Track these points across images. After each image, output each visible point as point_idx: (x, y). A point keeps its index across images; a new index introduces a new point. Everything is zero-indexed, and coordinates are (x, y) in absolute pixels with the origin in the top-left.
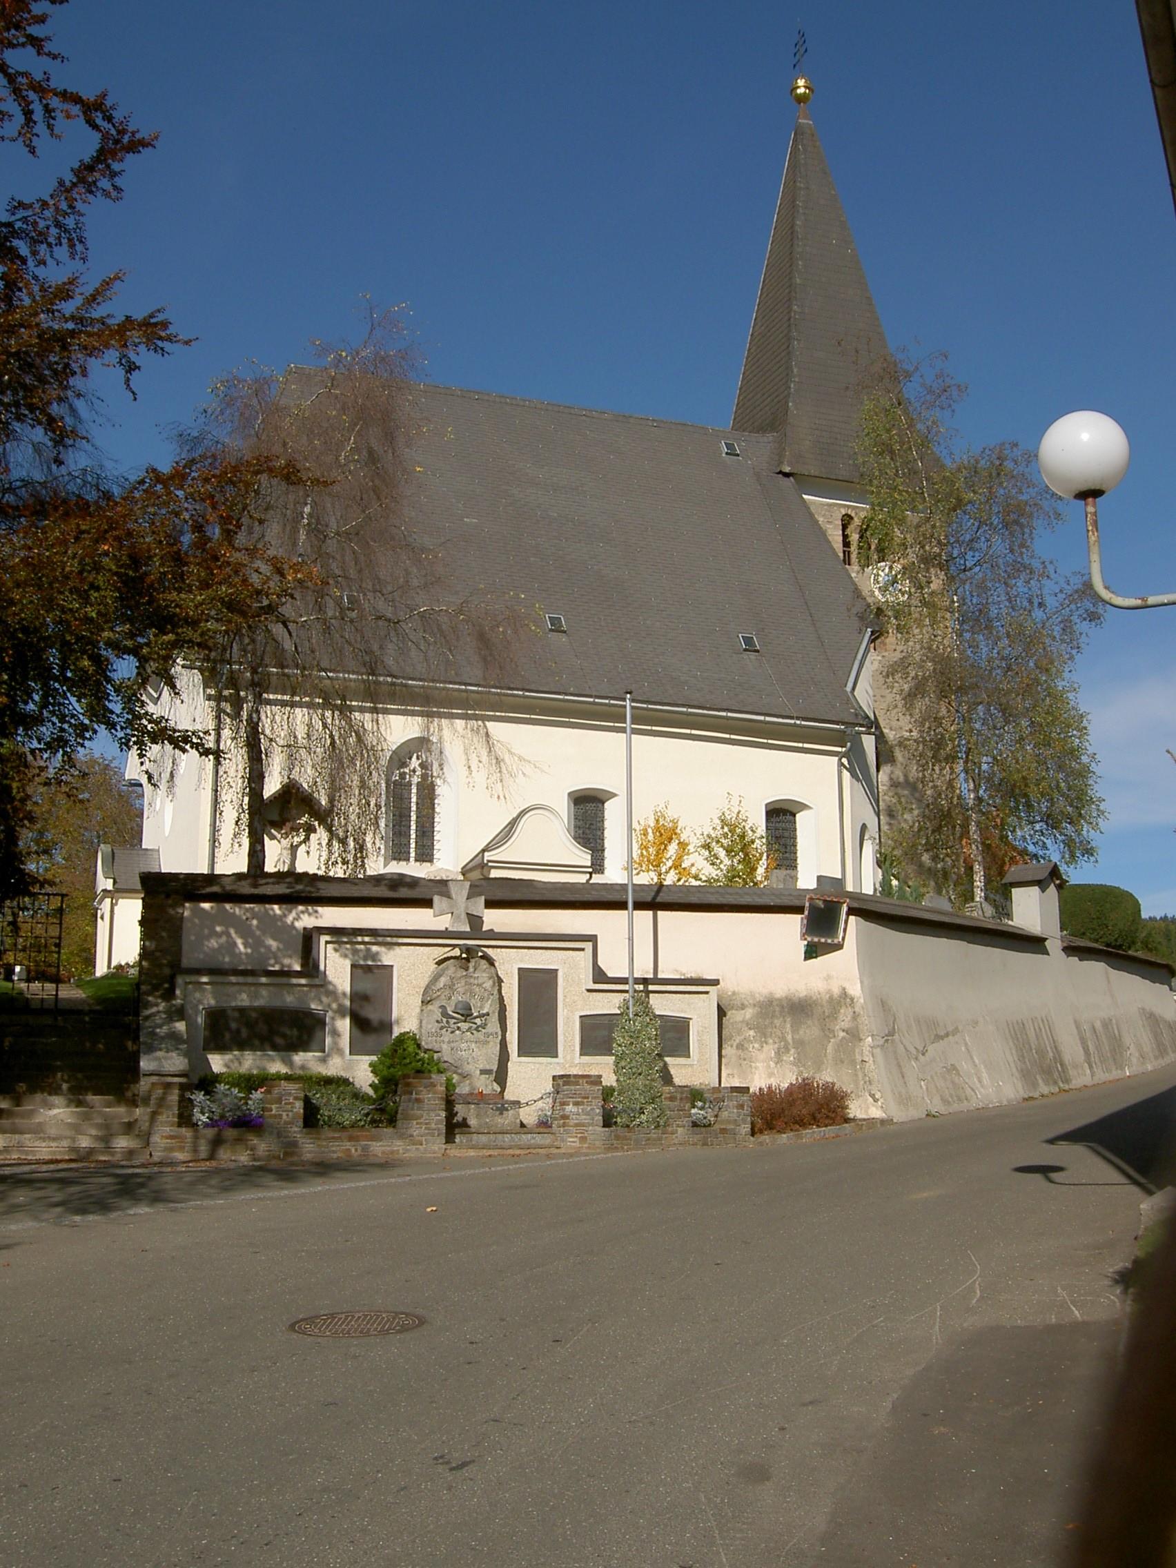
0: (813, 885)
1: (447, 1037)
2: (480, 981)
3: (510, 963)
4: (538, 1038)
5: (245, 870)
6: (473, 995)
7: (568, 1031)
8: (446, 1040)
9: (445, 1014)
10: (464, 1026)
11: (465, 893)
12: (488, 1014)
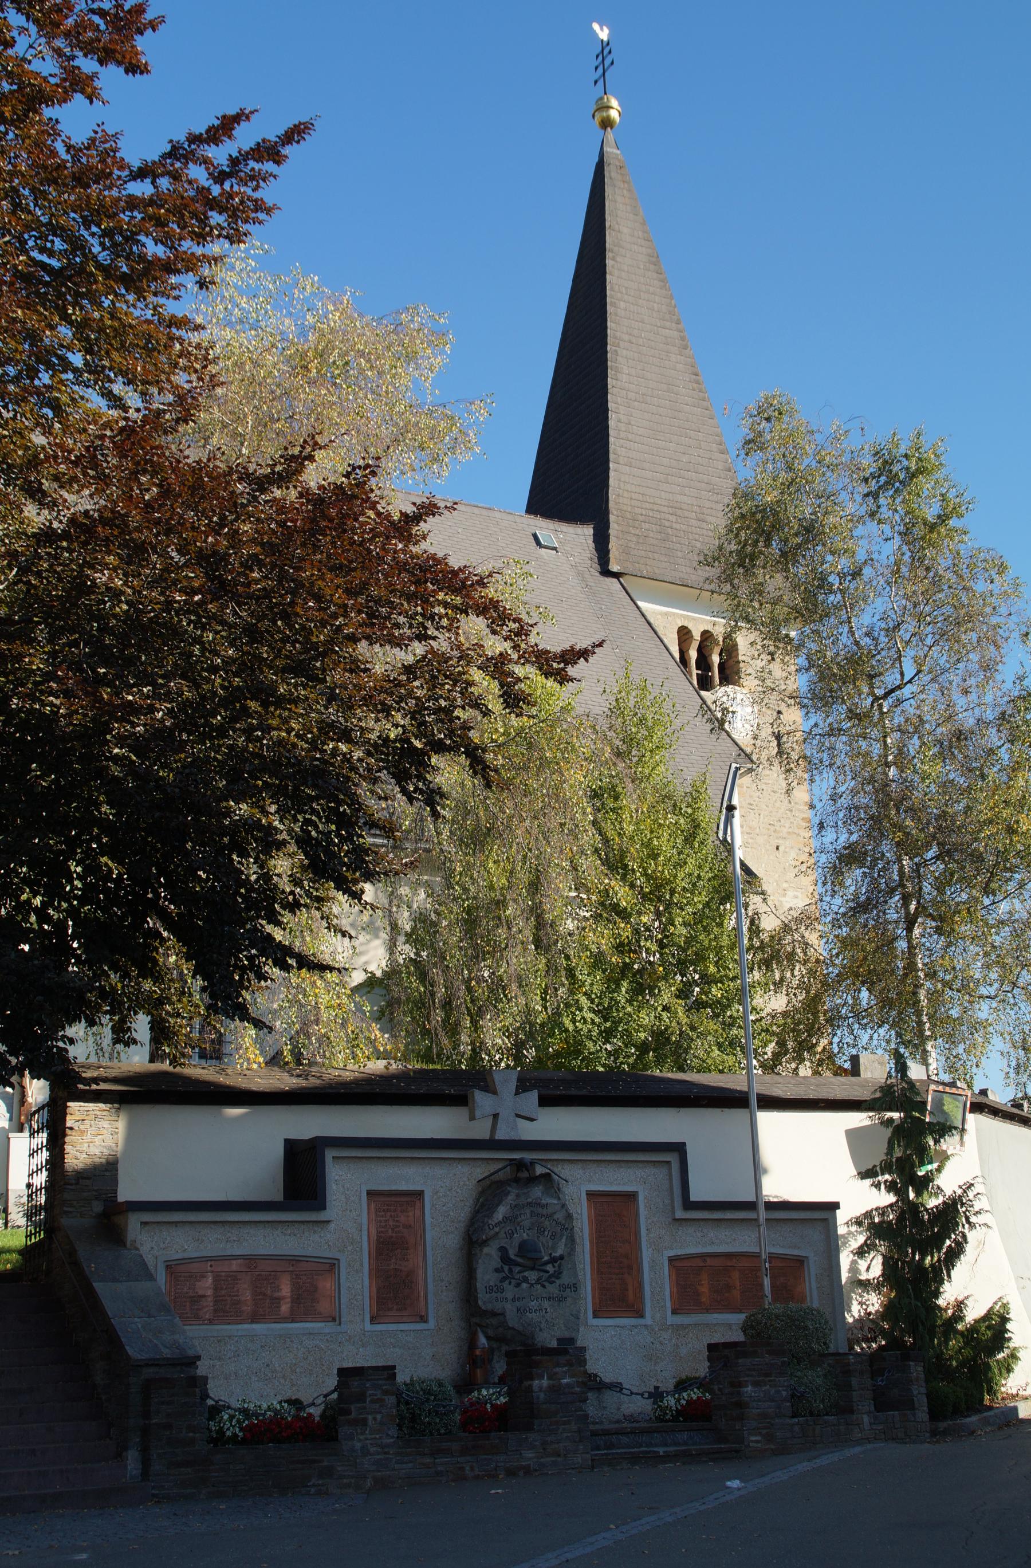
0: (79, 137)
1: (510, 1291)
2: (550, 1210)
3: (579, 1183)
4: (620, 1297)
5: (692, 1199)
6: (541, 1231)
7: (656, 1281)
8: (509, 1295)
9: (505, 1258)
10: (532, 1276)
11: (513, 1085)
12: (561, 1257)
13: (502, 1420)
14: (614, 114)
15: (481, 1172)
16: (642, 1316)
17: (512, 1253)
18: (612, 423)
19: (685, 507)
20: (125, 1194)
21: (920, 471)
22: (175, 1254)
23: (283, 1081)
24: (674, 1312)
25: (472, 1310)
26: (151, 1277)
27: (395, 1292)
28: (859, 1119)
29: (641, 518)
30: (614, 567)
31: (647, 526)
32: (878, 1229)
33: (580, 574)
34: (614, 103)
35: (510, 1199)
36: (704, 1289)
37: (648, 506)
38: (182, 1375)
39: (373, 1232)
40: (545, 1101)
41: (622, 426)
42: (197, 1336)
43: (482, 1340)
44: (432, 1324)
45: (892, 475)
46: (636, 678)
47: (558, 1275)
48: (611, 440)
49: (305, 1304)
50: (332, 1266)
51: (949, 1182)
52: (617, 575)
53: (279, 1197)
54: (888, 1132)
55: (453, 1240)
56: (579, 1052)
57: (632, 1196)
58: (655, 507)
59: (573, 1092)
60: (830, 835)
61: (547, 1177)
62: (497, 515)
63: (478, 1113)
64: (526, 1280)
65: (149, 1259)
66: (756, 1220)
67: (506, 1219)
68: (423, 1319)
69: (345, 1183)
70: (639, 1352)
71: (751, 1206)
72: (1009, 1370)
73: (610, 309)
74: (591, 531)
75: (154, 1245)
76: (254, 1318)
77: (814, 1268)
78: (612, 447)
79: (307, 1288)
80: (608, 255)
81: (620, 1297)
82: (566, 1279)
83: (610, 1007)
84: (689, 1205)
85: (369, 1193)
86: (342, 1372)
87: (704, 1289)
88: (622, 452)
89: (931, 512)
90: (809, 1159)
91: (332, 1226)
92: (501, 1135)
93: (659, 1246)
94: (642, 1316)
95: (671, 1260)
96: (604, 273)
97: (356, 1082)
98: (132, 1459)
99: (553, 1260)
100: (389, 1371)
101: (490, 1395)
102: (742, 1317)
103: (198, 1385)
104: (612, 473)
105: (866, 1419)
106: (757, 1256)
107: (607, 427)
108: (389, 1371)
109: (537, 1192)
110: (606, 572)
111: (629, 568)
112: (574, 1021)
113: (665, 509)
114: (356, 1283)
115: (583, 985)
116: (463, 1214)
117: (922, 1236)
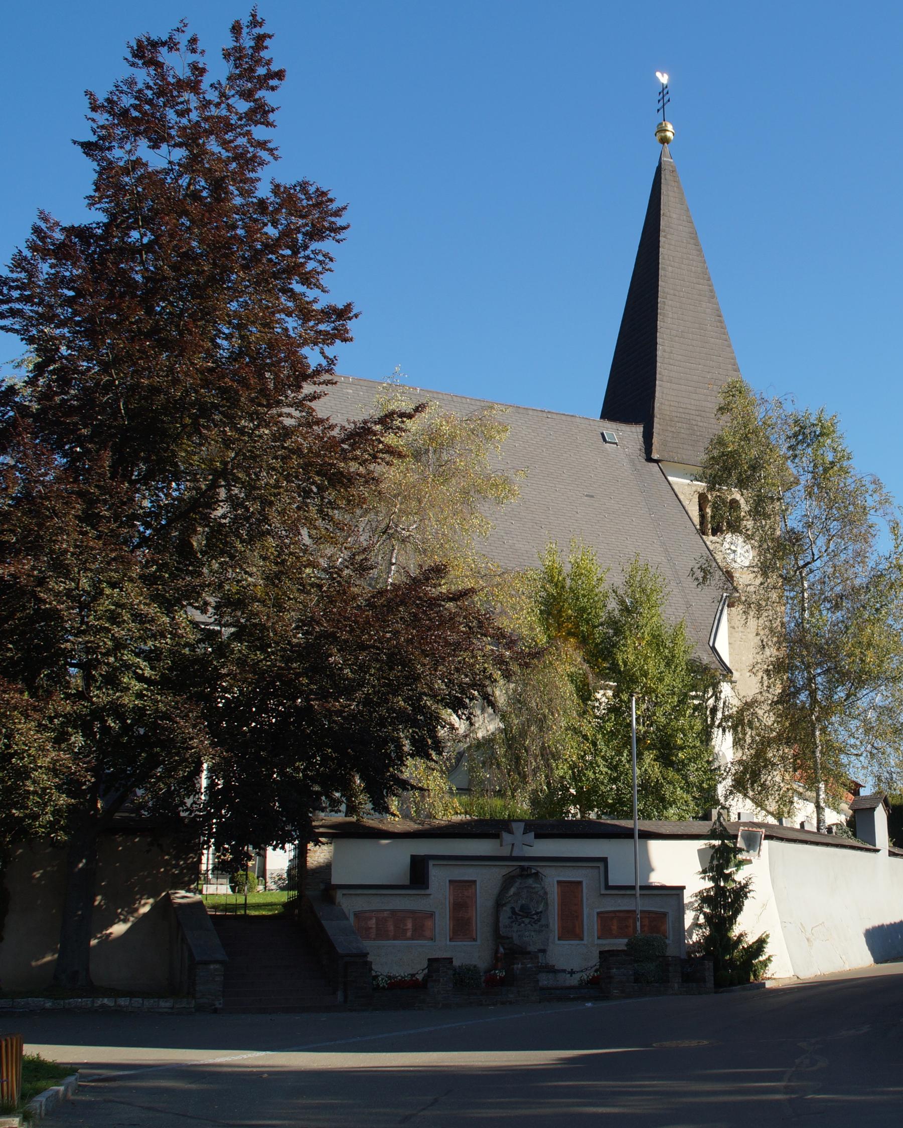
3: (552, 877)
4: (571, 929)
8: (515, 930)
10: (527, 920)
13: (503, 982)
14: (669, 135)
15: (505, 871)
16: (582, 940)
17: (517, 910)
18: (659, 353)
19: (708, 410)
20: (336, 880)
21: (822, 434)
22: (358, 908)
23: (412, 826)
24: (599, 938)
25: (498, 937)
26: (347, 919)
27: (461, 927)
28: (701, 844)
29: (676, 419)
30: (655, 456)
31: (680, 425)
32: (705, 899)
33: (632, 461)
34: (670, 127)
35: (517, 884)
36: (615, 928)
37: (681, 410)
38: (361, 961)
39: (452, 901)
40: (537, 836)
41: (666, 355)
42: (368, 945)
43: (501, 950)
44: (479, 942)
45: (806, 434)
46: (641, 562)
47: (539, 920)
48: (658, 364)
49: (419, 932)
50: (431, 915)
51: (740, 876)
52: (657, 461)
53: (407, 882)
54: (712, 852)
55: (490, 903)
56: (597, 792)
57: (580, 883)
58: (687, 411)
59: (555, 831)
60: (768, 652)
61: (537, 874)
62: (578, 420)
63: (504, 843)
64: (523, 922)
65: (346, 911)
66: (635, 895)
67: (514, 894)
68: (475, 940)
69: (438, 876)
70: (573, 957)
71: (633, 888)
72: (766, 966)
73: (661, 272)
74: (642, 429)
75: (349, 904)
76: (395, 938)
77: (670, 919)
78: (658, 369)
79: (420, 924)
80: (662, 234)
81: (571, 929)
82: (543, 922)
83: (617, 765)
84: (608, 887)
85: (450, 881)
86: (429, 960)
87: (615, 928)
88: (665, 373)
89: (830, 457)
90: (676, 864)
91: (432, 897)
92: (514, 854)
93: (591, 908)
94: (582, 940)
95: (598, 913)
96: (658, 247)
97: (446, 827)
98: (340, 995)
99: (537, 913)
100: (450, 960)
101: (500, 974)
102: (626, 940)
103: (368, 965)
104: (658, 388)
105: (676, 985)
106: (635, 911)
107: (656, 356)
108: (450, 960)
109: (530, 881)
110: (649, 459)
111: (666, 456)
112: (595, 773)
113: (693, 412)
114: (443, 923)
115: (601, 752)
116: (496, 891)
117: (725, 902)
